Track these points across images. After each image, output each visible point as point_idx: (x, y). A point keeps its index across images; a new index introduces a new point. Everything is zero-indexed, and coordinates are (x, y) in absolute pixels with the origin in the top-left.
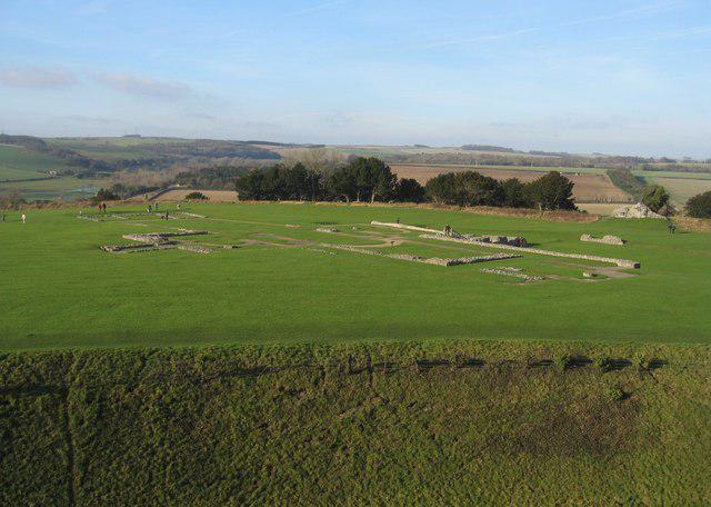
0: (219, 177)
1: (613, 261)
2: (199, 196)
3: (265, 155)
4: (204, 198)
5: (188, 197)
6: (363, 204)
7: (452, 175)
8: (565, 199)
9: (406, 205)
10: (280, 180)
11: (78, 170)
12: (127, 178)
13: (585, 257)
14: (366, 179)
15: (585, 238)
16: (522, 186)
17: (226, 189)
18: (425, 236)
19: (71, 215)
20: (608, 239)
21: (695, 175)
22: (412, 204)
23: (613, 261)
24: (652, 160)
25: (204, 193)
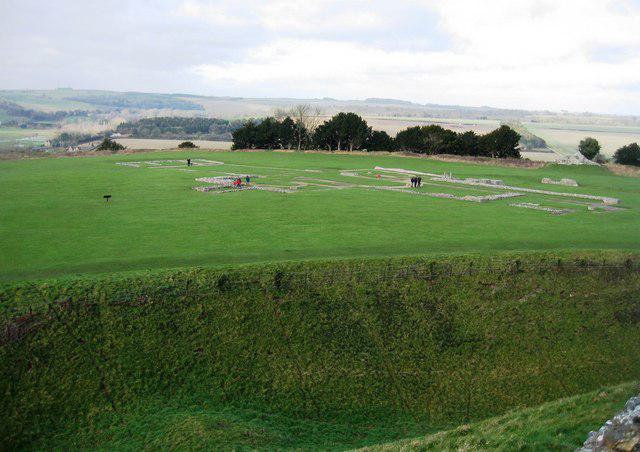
1: (599, 198)
2: (191, 145)
3: (190, 107)
6: (344, 152)
7: (418, 128)
8: (512, 149)
9: (381, 153)
10: (266, 135)
11: (21, 120)
12: (71, 128)
14: (347, 132)
17: (164, 138)
19: (109, 161)
20: (565, 181)
22: (386, 153)
23: (599, 198)
24: (536, 113)
25: (194, 142)
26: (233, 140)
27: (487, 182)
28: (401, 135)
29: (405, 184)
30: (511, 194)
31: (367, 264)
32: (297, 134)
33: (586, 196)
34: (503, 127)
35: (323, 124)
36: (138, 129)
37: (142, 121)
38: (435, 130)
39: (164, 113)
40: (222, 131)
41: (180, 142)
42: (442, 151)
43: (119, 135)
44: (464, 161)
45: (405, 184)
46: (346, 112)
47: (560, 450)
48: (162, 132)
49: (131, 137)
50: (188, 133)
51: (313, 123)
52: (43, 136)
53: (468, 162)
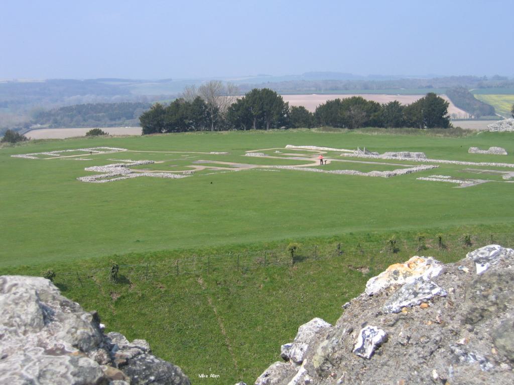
0: (119, 113)
4: (103, 133)
5: (88, 134)
8: (441, 118)
10: (176, 119)
13: (217, 153)
14: (261, 111)
15: (473, 150)
16: (403, 107)
18: (346, 154)
20: (493, 149)
21: (103, 175)
24: (485, 78)
25: (103, 129)
26: (141, 125)
27: (394, 156)
28: (322, 109)
29: (314, 162)
30: (423, 167)
31: (282, 241)
32: (209, 114)
33: (505, 165)
34: (430, 95)
35: (235, 102)
36: (59, 118)
37: (62, 109)
38: (357, 102)
39: (88, 99)
40: (130, 116)
41: (88, 130)
42: (366, 125)
43: (39, 126)
44: (388, 134)
45: (314, 162)
46: (260, 88)
47: (108, 383)
48: (85, 120)
49: (50, 127)
50: (111, 119)
51: (225, 102)
52: (124, 137)
53: (393, 135)
